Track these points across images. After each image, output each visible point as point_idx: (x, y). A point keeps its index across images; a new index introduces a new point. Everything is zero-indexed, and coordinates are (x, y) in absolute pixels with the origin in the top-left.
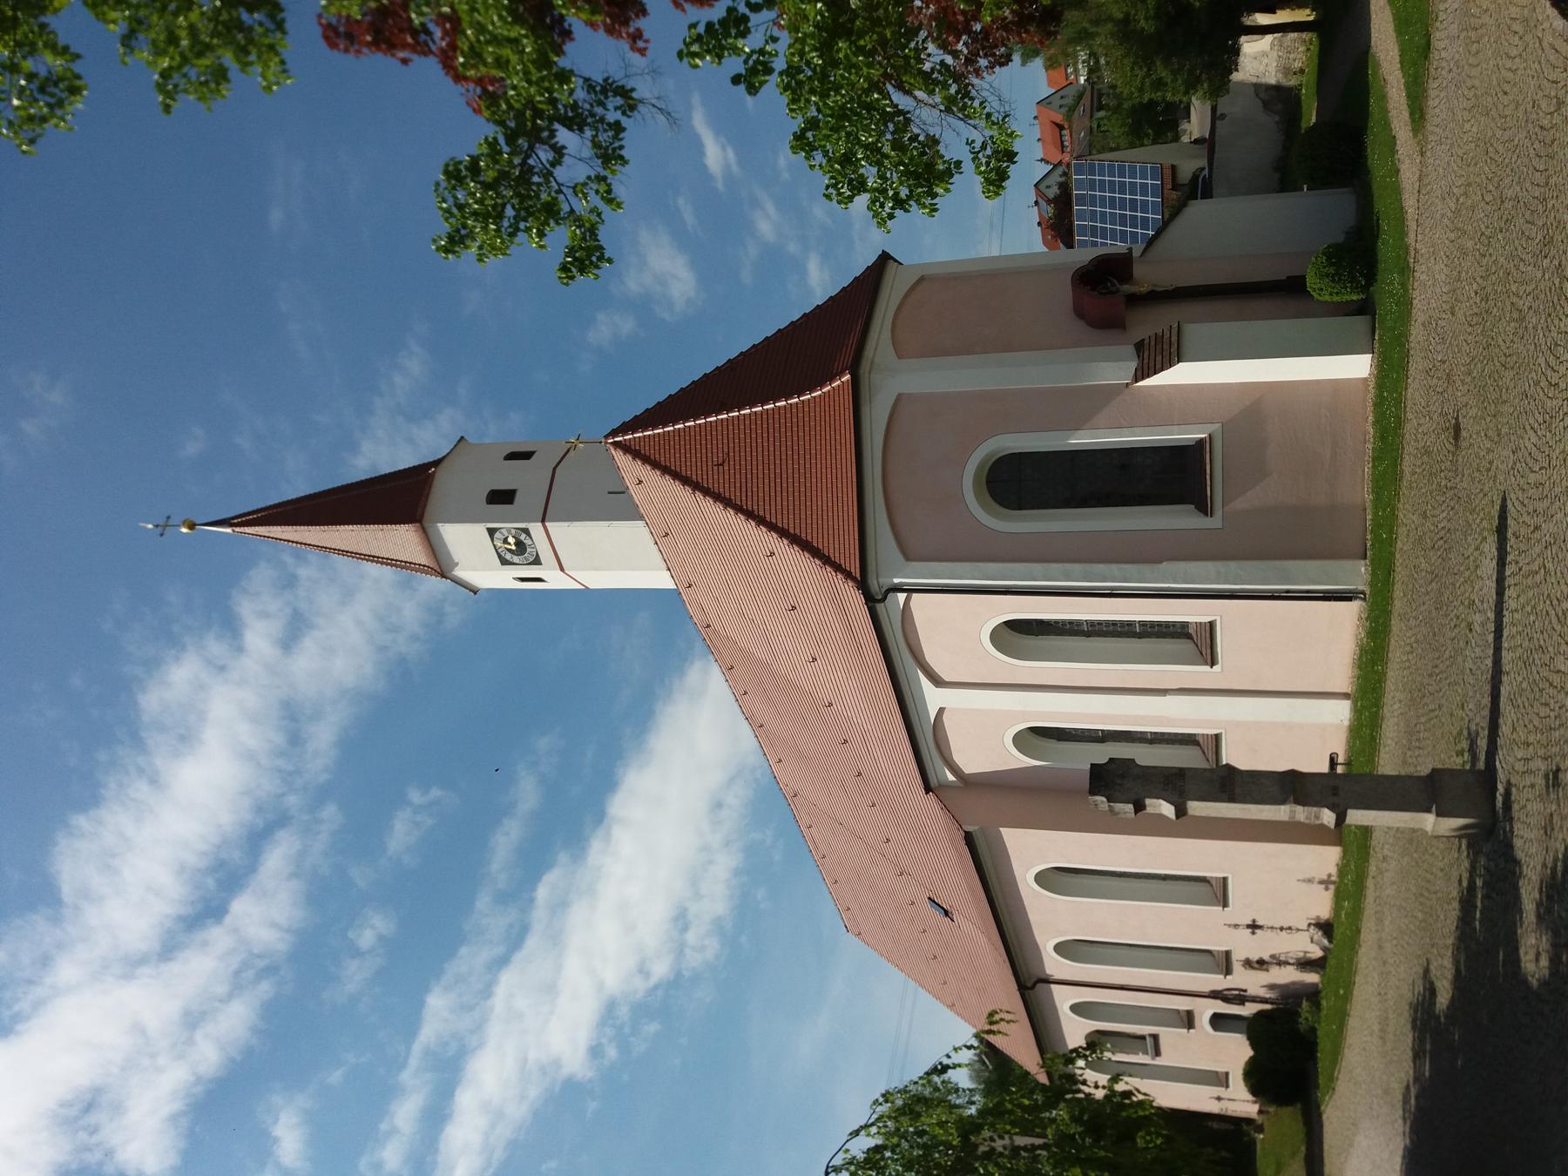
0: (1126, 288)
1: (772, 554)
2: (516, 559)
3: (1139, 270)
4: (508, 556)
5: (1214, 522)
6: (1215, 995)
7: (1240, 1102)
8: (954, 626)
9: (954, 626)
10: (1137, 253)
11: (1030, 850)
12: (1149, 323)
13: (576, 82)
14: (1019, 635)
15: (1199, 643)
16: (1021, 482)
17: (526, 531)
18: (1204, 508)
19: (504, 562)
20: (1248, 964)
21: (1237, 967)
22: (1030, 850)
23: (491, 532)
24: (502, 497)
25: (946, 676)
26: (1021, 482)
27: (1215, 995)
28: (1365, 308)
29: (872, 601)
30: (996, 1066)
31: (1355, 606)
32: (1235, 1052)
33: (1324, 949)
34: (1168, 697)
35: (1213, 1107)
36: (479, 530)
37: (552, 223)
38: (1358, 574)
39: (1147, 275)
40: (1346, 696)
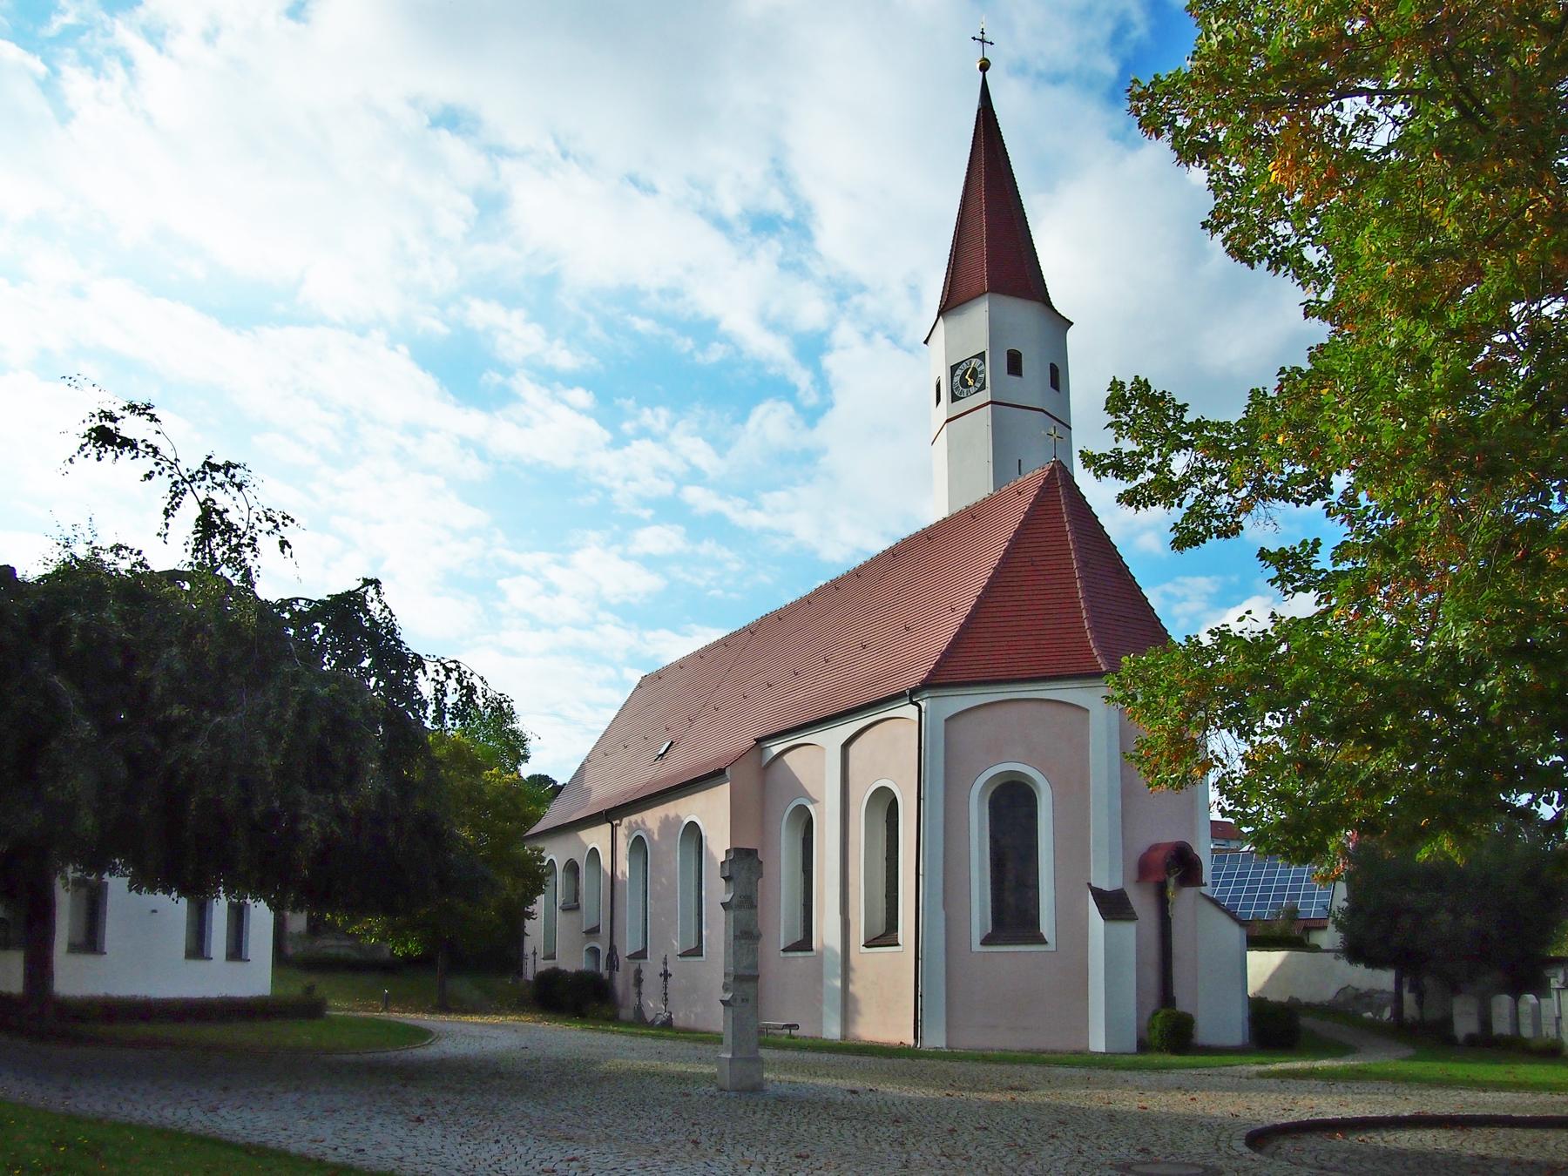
0: (1172, 881)
1: (953, 610)
2: (957, 379)
3: (1189, 893)
4: (959, 372)
5: (976, 946)
6: (612, 948)
7: (534, 965)
8: (891, 751)
9: (891, 751)
10: (1203, 890)
11: (711, 812)
12: (1143, 902)
13: (302, 602)
14: (885, 804)
15: (884, 936)
16: (1012, 805)
17: (983, 388)
18: (986, 941)
19: (954, 369)
20: (639, 972)
21: (633, 966)
22: (711, 812)
23: (981, 356)
24: (1014, 364)
25: (853, 749)
26: (1012, 805)
27: (612, 948)
28: (1143, 1047)
29: (914, 692)
30: (545, 789)
31: (911, 1042)
32: (572, 961)
33: (653, 1021)
34: (838, 917)
35: (528, 948)
36: (983, 345)
37: (1189, 418)
38: (936, 1039)
39: (1184, 901)
40: (844, 1037)
